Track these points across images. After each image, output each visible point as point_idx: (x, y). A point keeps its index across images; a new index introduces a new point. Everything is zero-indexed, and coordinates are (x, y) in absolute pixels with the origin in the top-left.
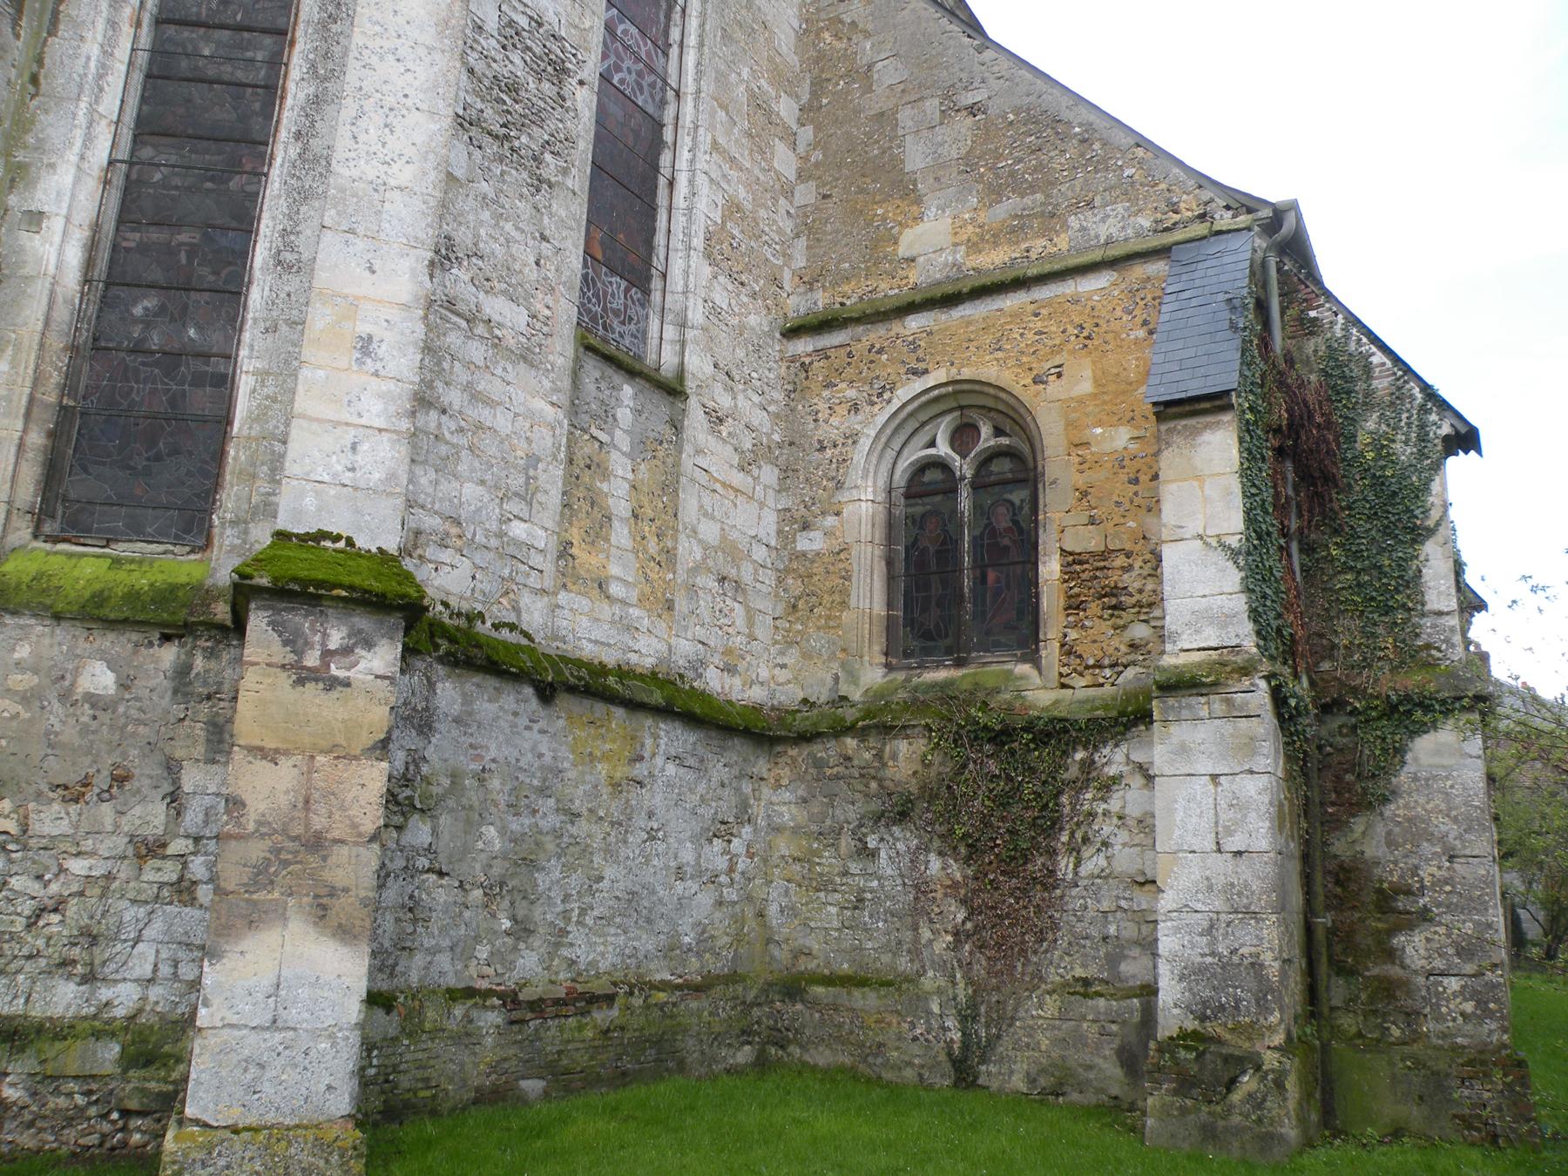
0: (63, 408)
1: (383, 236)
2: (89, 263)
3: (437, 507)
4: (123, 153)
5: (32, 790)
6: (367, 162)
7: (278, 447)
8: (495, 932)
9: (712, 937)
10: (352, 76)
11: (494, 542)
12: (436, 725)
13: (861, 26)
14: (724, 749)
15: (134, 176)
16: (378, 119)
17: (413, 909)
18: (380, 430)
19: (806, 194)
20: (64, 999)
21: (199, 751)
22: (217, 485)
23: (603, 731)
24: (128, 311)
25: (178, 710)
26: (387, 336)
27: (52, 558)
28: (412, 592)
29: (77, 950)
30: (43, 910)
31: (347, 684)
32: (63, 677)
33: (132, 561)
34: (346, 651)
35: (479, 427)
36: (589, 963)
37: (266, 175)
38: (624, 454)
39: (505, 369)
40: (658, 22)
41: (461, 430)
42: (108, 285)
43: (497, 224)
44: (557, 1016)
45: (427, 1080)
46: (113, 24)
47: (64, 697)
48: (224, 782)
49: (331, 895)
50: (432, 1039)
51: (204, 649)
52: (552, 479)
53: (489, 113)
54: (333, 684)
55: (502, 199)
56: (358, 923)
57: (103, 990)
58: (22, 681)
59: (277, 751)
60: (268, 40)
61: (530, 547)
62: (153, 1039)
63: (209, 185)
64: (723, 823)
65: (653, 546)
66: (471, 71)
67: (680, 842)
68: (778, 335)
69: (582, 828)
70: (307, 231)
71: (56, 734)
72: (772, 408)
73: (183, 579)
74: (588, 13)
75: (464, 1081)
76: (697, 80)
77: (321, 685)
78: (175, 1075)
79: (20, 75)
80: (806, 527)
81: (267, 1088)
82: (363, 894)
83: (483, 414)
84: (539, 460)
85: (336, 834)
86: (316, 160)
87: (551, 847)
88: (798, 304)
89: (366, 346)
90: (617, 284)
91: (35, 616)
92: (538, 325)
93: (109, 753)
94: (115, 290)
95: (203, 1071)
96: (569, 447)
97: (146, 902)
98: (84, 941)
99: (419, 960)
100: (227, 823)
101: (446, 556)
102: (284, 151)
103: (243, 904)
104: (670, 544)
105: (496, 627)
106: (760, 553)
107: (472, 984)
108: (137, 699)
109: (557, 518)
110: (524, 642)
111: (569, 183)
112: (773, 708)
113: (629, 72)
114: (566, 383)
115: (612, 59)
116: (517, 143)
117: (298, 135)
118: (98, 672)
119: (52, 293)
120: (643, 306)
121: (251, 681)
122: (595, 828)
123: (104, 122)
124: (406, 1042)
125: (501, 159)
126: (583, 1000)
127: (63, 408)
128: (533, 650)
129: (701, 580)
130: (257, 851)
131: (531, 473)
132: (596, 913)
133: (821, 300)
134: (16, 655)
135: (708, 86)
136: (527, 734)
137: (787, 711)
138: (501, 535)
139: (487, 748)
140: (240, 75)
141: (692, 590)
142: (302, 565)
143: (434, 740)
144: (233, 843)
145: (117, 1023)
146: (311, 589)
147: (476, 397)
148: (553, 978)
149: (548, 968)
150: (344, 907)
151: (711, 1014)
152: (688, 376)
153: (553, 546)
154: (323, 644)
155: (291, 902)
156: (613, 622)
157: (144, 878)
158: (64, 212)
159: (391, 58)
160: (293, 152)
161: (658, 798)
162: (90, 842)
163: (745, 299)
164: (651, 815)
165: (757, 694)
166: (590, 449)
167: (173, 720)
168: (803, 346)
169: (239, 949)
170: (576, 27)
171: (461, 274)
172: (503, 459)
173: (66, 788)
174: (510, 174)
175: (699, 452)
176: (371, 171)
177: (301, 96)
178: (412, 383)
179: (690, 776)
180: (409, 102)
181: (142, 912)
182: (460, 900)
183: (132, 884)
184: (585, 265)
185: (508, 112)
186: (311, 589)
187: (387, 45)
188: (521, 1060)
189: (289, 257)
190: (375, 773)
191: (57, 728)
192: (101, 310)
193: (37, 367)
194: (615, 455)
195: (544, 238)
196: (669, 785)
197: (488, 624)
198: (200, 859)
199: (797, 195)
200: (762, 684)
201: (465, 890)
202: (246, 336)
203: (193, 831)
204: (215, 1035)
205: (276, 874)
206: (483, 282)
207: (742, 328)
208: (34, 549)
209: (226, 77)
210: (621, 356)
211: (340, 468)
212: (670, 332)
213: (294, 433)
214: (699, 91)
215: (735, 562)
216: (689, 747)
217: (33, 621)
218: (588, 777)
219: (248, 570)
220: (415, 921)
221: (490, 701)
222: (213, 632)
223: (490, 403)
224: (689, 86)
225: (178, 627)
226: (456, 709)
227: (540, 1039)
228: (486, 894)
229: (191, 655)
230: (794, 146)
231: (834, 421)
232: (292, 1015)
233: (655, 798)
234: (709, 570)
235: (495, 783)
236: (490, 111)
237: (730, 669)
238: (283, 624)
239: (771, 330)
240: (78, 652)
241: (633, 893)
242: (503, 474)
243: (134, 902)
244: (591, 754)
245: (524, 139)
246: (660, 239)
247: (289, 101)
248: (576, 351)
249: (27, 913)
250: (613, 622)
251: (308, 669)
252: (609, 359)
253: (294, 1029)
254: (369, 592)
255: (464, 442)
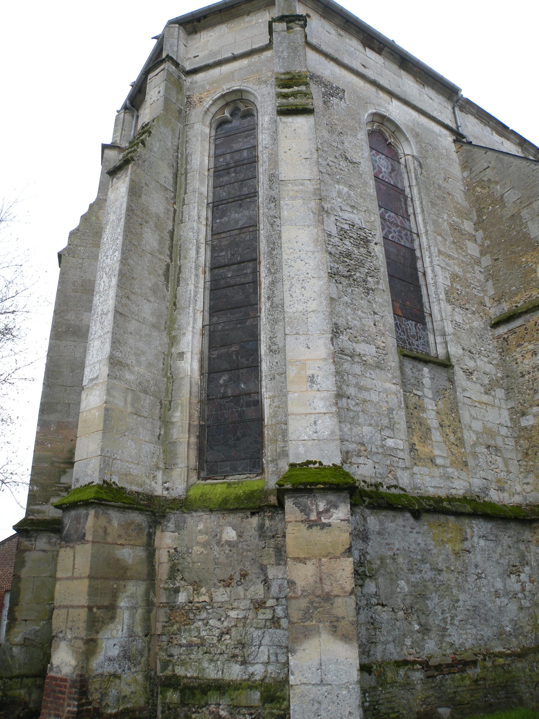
0: (201, 426)
1: (310, 332)
2: (201, 367)
3: (353, 439)
4: (207, 322)
5: (212, 583)
6: (298, 304)
7: (284, 427)
8: (413, 632)
9: (521, 627)
10: (286, 271)
11: (380, 450)
12: (370, 536)
13: (493, 180)
14: (506, 529)
15: (212, 329)
16: (299, 285)
17: (373, 623)
18: (324, 414)
19: (486, 261)
20: (235, 672)
21: (273, 560)
22: (262, 447)
23: (446, 528)
24: (218, 382)
25: (262, 544)
26: (321, 373)
27: (205, 487)
28: (350, 481)
29: (237, 650)
30: (223, 633)
31: (329, 525)
32: (217, 535)
33: (235, 483)
34: (327, 511)
35: (365, 401)
36: (460, 644)
37: (259, 317)
38: (430, 399)
39: (370, 374)
40: (402, 208)
41: (357, 404)
42: (209, 374)
43: (354, 313)
44: (450, 673)
45: (393, 708)
46: (197, 276)
47: (218, 543)
48: (285, 572)
49: (337, 621)
50: (392, 687)
51: (269, 517)
52: (400, 417)
53: (341, 268)
54: (324, 526)
55: (354, 302)
56: (351, 633)
57: (250, 668)
58: (202, 538)
59: (305, 558)
60: (251, 264)
61: (397, 449)
62: (272, 690)
63: (239, 326)
64: (514, 566)
65: (452, 438)
66: (330, 253)
67: (494, 578)
68: (489, 328)
69: (444, 576)
70: (280, 335)
71: (218, 559)
72: (494, 362)
73: (256, 488)
74: (372, 215)
75: (410, 708)
76: (425, 227)
77: (319, 527)
78: (283, 707)
79: (170, 304)
80: (523, 414)
81: (323, 713)
82: (351, 619)
83: (365, 395)
84: (393, 410)
85: (335, 593)
86: (277, 306)
87: (431, 587)
88: (495, 312)
89: (312, 379)
90: (411, 324)
91: (203, 511)
92: (381, 351)
93: (238, 564)
94: (212, 375)
95: (296, 705)
96: (405, 401)
97: (261, 628)
98: (240, 646)
99: (380, 648)
100: (289, 592)
101: (361, 460)
102: (264, 306)
103: (301, 628)
104: (460, 435)
105: (388, 488)
106: (504, 431)
107: (406, 658)
108: (246, 541)
109: (406, 434)
110: (402, 492)
111: (381, 287)
112: (527, 505)
113: (395, 232)
114: (398, 373)
115: (387, 229)
116: (355, 277)
117: (269, 298)
118: (229, 531)
119: (191, 381)
120: (424, 330)
121: (290, 529)
122: (451, 576)
123: (199, 312)
124: (380, 689)
125: (350, 285)
126: (461, 664)
127: (201, 426)
128: (407, 495)
129: (478, 450)
130: (303, 603)
131: (391, 416)
132: (459, 618)
133: (506, 307)
134: (199, 528)
135: (430, 228)
136: (411, 535)
137: (534, 506)
138: (383, 446)
139: (394, 544)
140: (243, 280)
141: (475, 455)
142: (303, 477)
143: (370, 544)
144: (293, 601)
145: (257, 682)
146: (308, 487)
147: (361, 388)
148: (444, 653)
149: (440, 648)
150: (344, 625)
151: (530, 670)
152: (452, 357)
153: (407, 446)
154: (317, 509)
155: (321, 625)
156: (441, 477)
157: (259, 617)
158: (190, 350)
159: (299, 260)
160: (268, 305)
161: (479, 557)
162: (236, 603)
163: (470, 316)
164: (476, 566)
165: (517, 499)
166: (415, 400)
167: (261, 548)
168: (502, 330)
169: (302, 648)
170: (368, 222)
171: (344, 337)
172: (377, 412)
173: (224, 581)
174: (355, 290)
175: (464, 390)
176: (300, 307)
177: (267, 282)
178: (334, 391)
179: (492, 545)
180: (309, 276)
181: (260, 632)
182: (393, 617)
183: (255, 621)
184: (395, 320)
185: (349, 265)
186: (308, 487)
187: (296, 255)
188: (436, 697)
189: (274, 347)
190: (348, 563)
191: (217, 556)
192: (208, 384)
193: (190, 411)
194: (426, 400)
195: (375, 313)
196: (483, 550)
197: (385, 487)
198: (280, 608)
199: (482, 262)
200: (519, 494)
201: (395, 612)
202: (264, 383)
203: (275, 595)
204: (298, 688)
205: (313, 613)
206: (354, 339)
207: (471, 329)
208: (199, 484)
209: (238, 283)
210: (419, 355)
211: (311, 433)
212: (439, 339)
213: (290, 422)
214: (427, 231)
215: (493, 437)
216: (489, 531)
217: (202, 514)
218: (443, 552)
219: (281, 483)
220: (375, 629)
221: (391, 522)
222: (271, 509)
223: (367, 390)
224: (422, 230)
225: (257, 509)
226: (377, 528)
227: (443, 686)
228: (405, 613)
229: (263, 520)
230: (475, 241)
231: (526, 361)
232: (330, 678)
233: (477, 557)
234: (481, 444)
235: (400, 560)
236: (341, 267)
237: (501, 489)
238: (299, 503)
239: (486, 327)
240: (221, 524)
241: (475, 606)
242: (379, 419)
243: (256, 628)
244: (442, 540)
245: (358, 274)
246: (425, 299)
247: (263, 286)
248: (399, 358)
249: (217, 635)
250: (441, 477)
251: (313, 521)
252: (415, 358)
253: (331, 685)
254: (333, 484)
255: (359, 409)
